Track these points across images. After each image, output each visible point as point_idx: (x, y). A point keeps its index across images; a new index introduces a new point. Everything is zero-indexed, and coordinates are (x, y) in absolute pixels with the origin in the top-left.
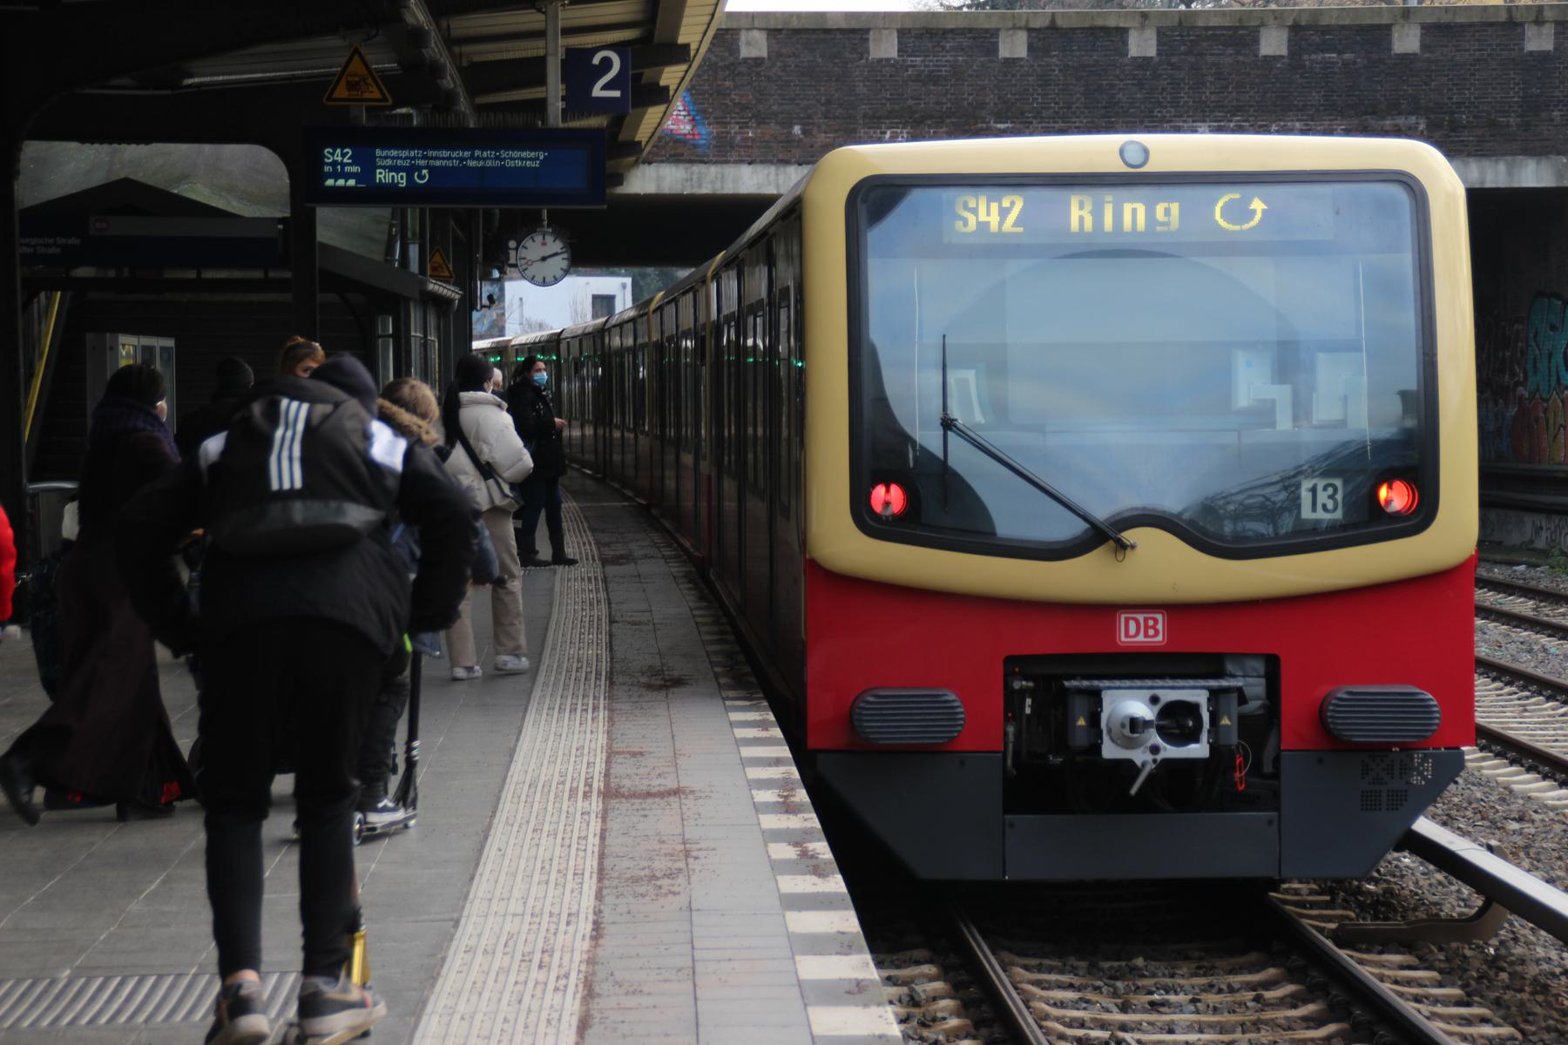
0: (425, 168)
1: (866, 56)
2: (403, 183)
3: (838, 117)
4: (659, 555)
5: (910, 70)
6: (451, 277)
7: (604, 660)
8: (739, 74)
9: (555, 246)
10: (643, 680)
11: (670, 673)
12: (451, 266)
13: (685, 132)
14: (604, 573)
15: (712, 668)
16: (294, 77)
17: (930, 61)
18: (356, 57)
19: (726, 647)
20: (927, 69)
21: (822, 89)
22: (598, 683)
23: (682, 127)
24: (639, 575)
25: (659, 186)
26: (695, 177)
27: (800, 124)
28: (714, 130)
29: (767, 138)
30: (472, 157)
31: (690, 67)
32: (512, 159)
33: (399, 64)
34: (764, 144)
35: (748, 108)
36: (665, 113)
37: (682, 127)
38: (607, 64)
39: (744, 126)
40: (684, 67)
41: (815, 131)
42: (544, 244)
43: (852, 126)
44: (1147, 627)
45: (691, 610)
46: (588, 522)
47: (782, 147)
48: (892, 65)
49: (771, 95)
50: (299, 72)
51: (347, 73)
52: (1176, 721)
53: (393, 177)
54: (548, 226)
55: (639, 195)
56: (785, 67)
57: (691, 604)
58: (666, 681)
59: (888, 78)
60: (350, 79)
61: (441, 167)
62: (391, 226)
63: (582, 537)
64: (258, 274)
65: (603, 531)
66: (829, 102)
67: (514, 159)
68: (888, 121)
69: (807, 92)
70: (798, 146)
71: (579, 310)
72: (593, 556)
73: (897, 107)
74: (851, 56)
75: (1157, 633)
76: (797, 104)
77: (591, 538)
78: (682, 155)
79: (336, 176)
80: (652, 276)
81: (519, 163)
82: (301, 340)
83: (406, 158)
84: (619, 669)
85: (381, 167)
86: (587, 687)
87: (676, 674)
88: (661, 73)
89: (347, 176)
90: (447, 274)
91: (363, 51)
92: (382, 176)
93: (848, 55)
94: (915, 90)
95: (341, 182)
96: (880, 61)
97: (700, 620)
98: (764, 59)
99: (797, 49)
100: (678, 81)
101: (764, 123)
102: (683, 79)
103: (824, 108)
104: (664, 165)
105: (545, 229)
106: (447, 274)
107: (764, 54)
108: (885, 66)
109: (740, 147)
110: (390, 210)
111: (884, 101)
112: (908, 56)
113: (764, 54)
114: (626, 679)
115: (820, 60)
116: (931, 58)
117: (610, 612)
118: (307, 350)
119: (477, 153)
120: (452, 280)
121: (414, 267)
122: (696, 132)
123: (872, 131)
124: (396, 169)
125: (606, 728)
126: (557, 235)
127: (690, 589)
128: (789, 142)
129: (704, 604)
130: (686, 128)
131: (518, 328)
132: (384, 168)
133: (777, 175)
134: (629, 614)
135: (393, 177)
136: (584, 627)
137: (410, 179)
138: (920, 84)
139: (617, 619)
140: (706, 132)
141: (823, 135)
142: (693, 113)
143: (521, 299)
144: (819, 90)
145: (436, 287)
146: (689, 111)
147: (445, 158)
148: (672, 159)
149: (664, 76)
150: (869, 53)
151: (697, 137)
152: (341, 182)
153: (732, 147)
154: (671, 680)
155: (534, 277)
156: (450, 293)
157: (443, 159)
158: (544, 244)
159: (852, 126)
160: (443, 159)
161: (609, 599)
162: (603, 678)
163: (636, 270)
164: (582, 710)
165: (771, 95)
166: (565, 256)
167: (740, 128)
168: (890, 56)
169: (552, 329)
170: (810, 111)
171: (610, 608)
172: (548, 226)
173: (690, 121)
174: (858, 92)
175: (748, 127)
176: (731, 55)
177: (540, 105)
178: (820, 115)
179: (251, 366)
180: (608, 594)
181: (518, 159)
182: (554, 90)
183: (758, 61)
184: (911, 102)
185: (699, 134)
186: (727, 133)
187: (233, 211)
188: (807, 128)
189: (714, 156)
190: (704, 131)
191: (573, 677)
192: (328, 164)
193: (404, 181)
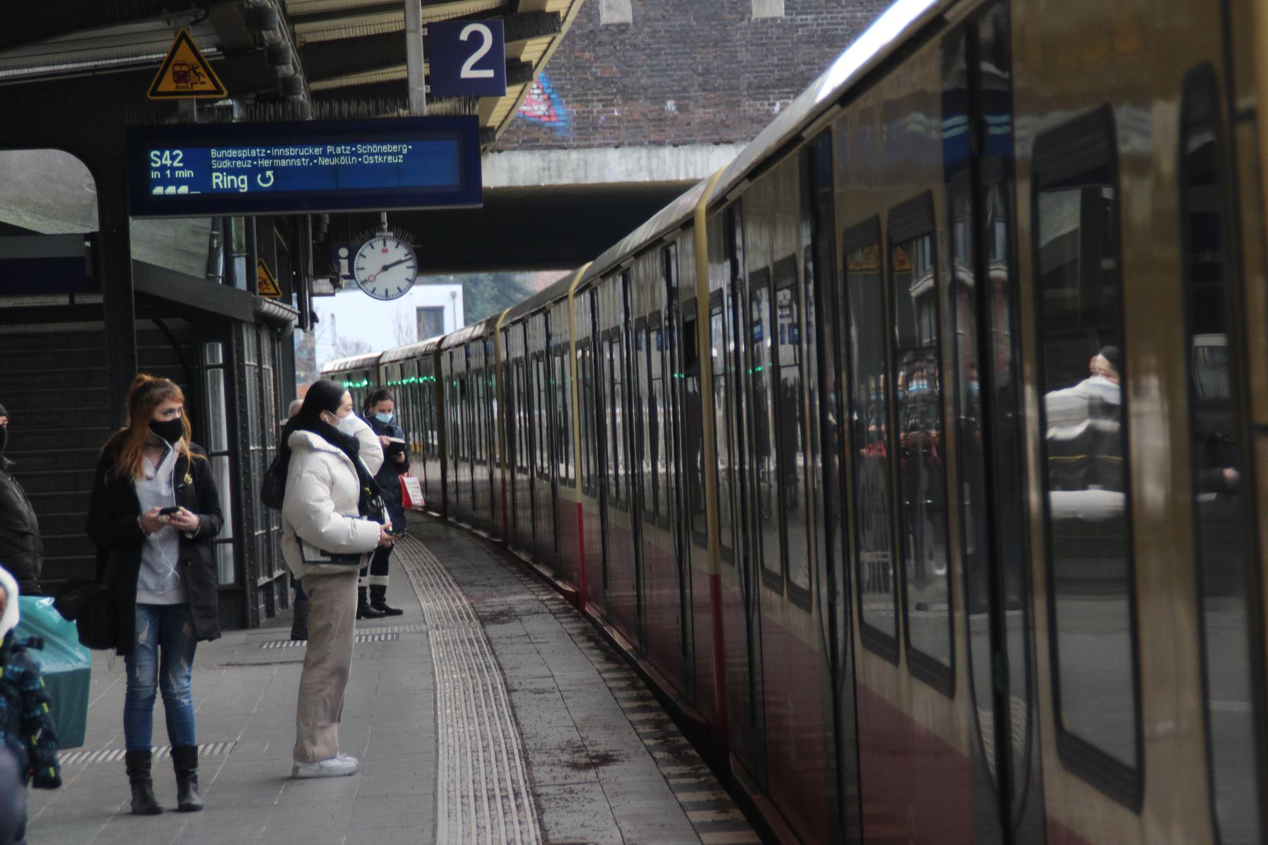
0: (269, 169)
1: (747, 16)
2: (244, 188)
3: (716, 89)
4: (545, 610)
5: (800, 29)
6: (278, 293)
7: (512, 735)
8: (600, 42)
9: (398, 252)
10: (565, 757)
11: (595, 749)
12: (276, 281)
13: (540, 113)
14: (485, 633)
15: (641, 740)
16: (96, 69)
17: (823, 19)
18: (184, 44)
19: (652, 715)
20: (819, 28)
21: (699, 56)
22: (512, 764)
23: (536, 108)
24: (528, 635)
25: (511, 178)
26: (553, 165)
27: (675, 99)
28: (574, 109)
29: (636, 116)
30: (324, 154)
31: (554, 38)
32: (370, 154)
33: (219, 48)
34: (632, 124)
35: (612, 82)
36: (522, 92)
37: (536, 108)
38: (476, 39)
39: (608, 103)
40: (547, 39)
41: (692, 107)
42: (385, 251)
43: (735, 99)
45: (600, 673)
46: (451, 574)
47: (654, 126)
48: (778, 26)
49: (639, 66)
50: (116, 61)
51: (174, 62)
53: (232, 181)
54: (389, 229)
55: (490, 188)
56: (654, 33)
57: (598, 666)
58: (592, 758)
59: (775, 40)
60: (177, 68)
61: (287, 168)
62: (212, 237)
63: (448, 592)
64: (63, 300)
65: (472, 584)
66: (707, 71)
67: (373, 155)
68: (776, 91)
69: (680, 61)
70: (673, 124)
71: (404, 325)
72: (468, 615)
73: (786, 74)
74: (730, 17)
76: (670, 76)
77: (460, 593)
78: (537, 140)
79: (165, 182)
80: (486, 282)
81: (379, 159)
82: (148, 378)
83: (247, 158)
84: (533, 747)
85: (217, 170)
86: (501, 770)
87: (602, 749)
88: (523, 46)
89: (178, 182)
90: (273, 291)
91: (191, 35)
92: (220, 181)
93: (727, 16)
94: (809, 53)
96: (764, 21)
97: (612, 684)
98: (627, 25)
99: (667, 11)
100: (539, 54)
101: (632, 99)
102: (545, 52)
103: (701, 79)
104: (516, 153)
105: (386, 233)
106: (273, 291)
107: (628, 18)
108: (771, 27)
109: (604, 128)
110: (210, 219)
111: (771, 68)
112: (798, 14)
113: (628, 18)
114: (544, 758)
115: (695, 23)
116: (824, 15)
117: (505, 680)
118: (164, 390)
119: (330, 149)
120: (278, 297)
121: (241, 283)
122: (552, 113)
123: (758, 103)
124: (235, 172)
125: (535, 817)
126: (400, 239)
127: (591, 648)
128: (660, 120)
129: (612, 666)
130: (540, 109)
131: (332, 351)
132: (221, 171)
133: (649, 159)
134: (529, 681)
135: (232, 181)
136: (479, 698)
137: (252, 181)
138: (813, 46)
139: (516, 687)
140: (564, 113)
141: (701, 110)
142: (548, 91)
143: (333, 316)
144: (695, 58)
145: (272, 307)
146: (543, 89)
147: (293, 156)
148: (525, 145)
149: (527, 49)
150: (751, 13)
151: (553, 119)
152: (171, 190)
153: (595, 128)
154: (596, 757)
155: (374, 290)
156: (286, 312)
157: (290, 157)
158: (385, 251)
159: (735, 99)
160: (290, 157)
161: (499, 664)
162: (517, 758)
163: (466, 276)
164: (502, 797)
165: (639, 66)
166: (410, 263)
167: (604, 106)
168: (775, 15)
169: (370, 351)
170: (685, 84)
171: (503, 674)
172: (389, 229)
173: (545, 100)
174: (740, 58)
175: (613, 105)
176: (590, 21)
177: (400, 89)
178: (696, 87)
180: (496, 658)
181: (377, 154)
182: (416, 69)
183: (622, 28)
184: (803, 67)
185: (556, 116)
186: (590, 112)
187: (26, 227)
188: (682, 102)
189: (574, 140)
190: (561, 112)
191: (481, 759)
192: (156, 169)
193: (246, 185)
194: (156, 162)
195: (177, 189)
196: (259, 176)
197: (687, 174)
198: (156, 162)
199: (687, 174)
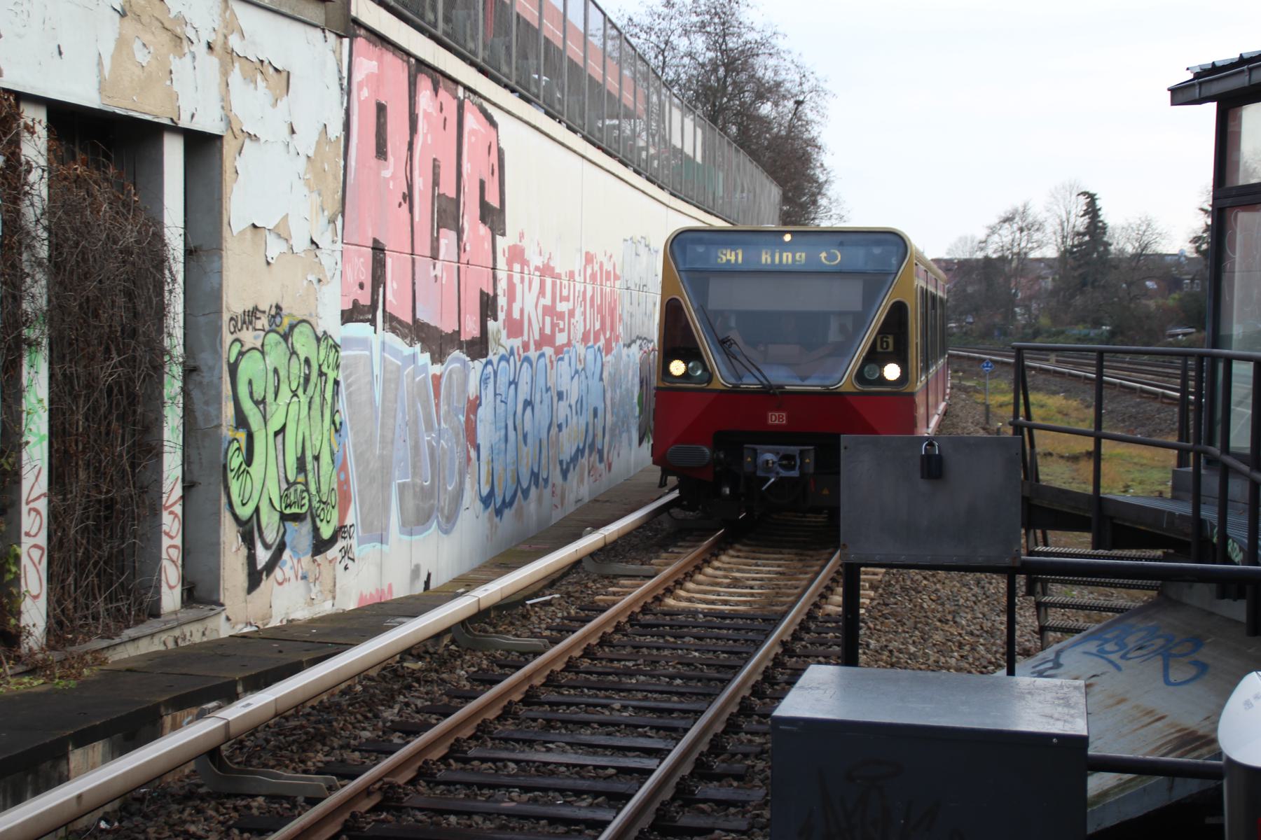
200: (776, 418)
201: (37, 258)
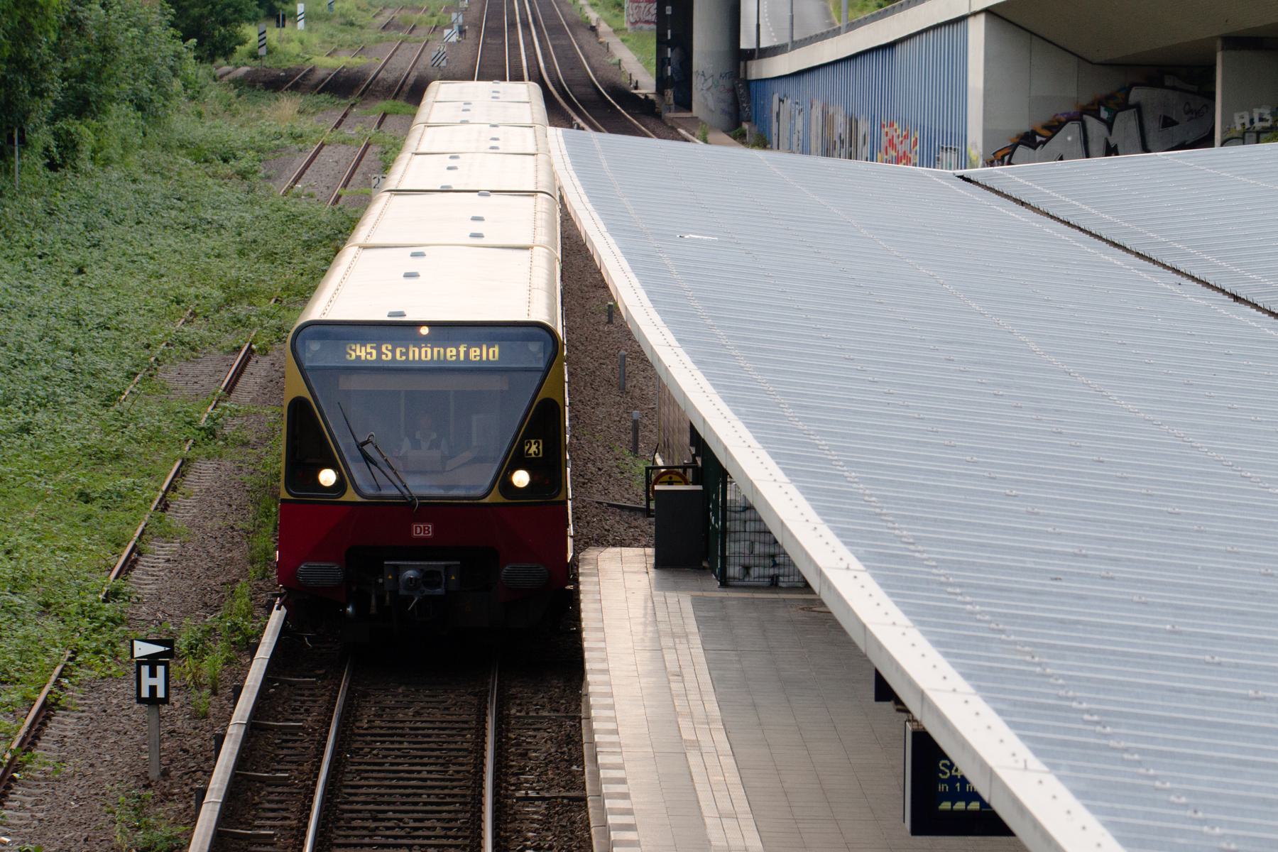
44: (425, 530)
52: (429, 578)
75: (429, 532)
95: (960, 805)
152: (960, 805)
179: (683, 129)
192: (943, 781)
194: (945, 773)
195: (953, 805)
196: (940, 775)
197: (592, 649)
198: (945, 773)
199: (592, 649)
200: (422, 531)
201: (75, 77)
